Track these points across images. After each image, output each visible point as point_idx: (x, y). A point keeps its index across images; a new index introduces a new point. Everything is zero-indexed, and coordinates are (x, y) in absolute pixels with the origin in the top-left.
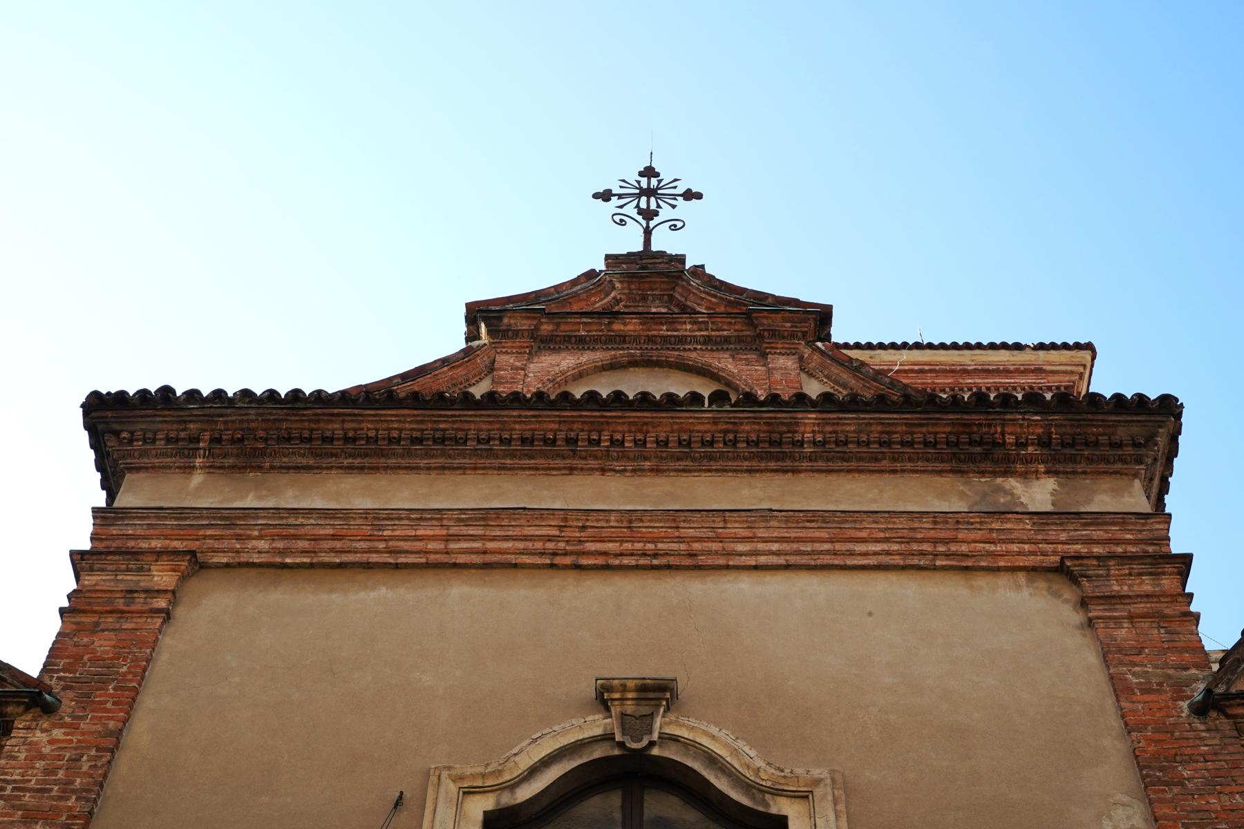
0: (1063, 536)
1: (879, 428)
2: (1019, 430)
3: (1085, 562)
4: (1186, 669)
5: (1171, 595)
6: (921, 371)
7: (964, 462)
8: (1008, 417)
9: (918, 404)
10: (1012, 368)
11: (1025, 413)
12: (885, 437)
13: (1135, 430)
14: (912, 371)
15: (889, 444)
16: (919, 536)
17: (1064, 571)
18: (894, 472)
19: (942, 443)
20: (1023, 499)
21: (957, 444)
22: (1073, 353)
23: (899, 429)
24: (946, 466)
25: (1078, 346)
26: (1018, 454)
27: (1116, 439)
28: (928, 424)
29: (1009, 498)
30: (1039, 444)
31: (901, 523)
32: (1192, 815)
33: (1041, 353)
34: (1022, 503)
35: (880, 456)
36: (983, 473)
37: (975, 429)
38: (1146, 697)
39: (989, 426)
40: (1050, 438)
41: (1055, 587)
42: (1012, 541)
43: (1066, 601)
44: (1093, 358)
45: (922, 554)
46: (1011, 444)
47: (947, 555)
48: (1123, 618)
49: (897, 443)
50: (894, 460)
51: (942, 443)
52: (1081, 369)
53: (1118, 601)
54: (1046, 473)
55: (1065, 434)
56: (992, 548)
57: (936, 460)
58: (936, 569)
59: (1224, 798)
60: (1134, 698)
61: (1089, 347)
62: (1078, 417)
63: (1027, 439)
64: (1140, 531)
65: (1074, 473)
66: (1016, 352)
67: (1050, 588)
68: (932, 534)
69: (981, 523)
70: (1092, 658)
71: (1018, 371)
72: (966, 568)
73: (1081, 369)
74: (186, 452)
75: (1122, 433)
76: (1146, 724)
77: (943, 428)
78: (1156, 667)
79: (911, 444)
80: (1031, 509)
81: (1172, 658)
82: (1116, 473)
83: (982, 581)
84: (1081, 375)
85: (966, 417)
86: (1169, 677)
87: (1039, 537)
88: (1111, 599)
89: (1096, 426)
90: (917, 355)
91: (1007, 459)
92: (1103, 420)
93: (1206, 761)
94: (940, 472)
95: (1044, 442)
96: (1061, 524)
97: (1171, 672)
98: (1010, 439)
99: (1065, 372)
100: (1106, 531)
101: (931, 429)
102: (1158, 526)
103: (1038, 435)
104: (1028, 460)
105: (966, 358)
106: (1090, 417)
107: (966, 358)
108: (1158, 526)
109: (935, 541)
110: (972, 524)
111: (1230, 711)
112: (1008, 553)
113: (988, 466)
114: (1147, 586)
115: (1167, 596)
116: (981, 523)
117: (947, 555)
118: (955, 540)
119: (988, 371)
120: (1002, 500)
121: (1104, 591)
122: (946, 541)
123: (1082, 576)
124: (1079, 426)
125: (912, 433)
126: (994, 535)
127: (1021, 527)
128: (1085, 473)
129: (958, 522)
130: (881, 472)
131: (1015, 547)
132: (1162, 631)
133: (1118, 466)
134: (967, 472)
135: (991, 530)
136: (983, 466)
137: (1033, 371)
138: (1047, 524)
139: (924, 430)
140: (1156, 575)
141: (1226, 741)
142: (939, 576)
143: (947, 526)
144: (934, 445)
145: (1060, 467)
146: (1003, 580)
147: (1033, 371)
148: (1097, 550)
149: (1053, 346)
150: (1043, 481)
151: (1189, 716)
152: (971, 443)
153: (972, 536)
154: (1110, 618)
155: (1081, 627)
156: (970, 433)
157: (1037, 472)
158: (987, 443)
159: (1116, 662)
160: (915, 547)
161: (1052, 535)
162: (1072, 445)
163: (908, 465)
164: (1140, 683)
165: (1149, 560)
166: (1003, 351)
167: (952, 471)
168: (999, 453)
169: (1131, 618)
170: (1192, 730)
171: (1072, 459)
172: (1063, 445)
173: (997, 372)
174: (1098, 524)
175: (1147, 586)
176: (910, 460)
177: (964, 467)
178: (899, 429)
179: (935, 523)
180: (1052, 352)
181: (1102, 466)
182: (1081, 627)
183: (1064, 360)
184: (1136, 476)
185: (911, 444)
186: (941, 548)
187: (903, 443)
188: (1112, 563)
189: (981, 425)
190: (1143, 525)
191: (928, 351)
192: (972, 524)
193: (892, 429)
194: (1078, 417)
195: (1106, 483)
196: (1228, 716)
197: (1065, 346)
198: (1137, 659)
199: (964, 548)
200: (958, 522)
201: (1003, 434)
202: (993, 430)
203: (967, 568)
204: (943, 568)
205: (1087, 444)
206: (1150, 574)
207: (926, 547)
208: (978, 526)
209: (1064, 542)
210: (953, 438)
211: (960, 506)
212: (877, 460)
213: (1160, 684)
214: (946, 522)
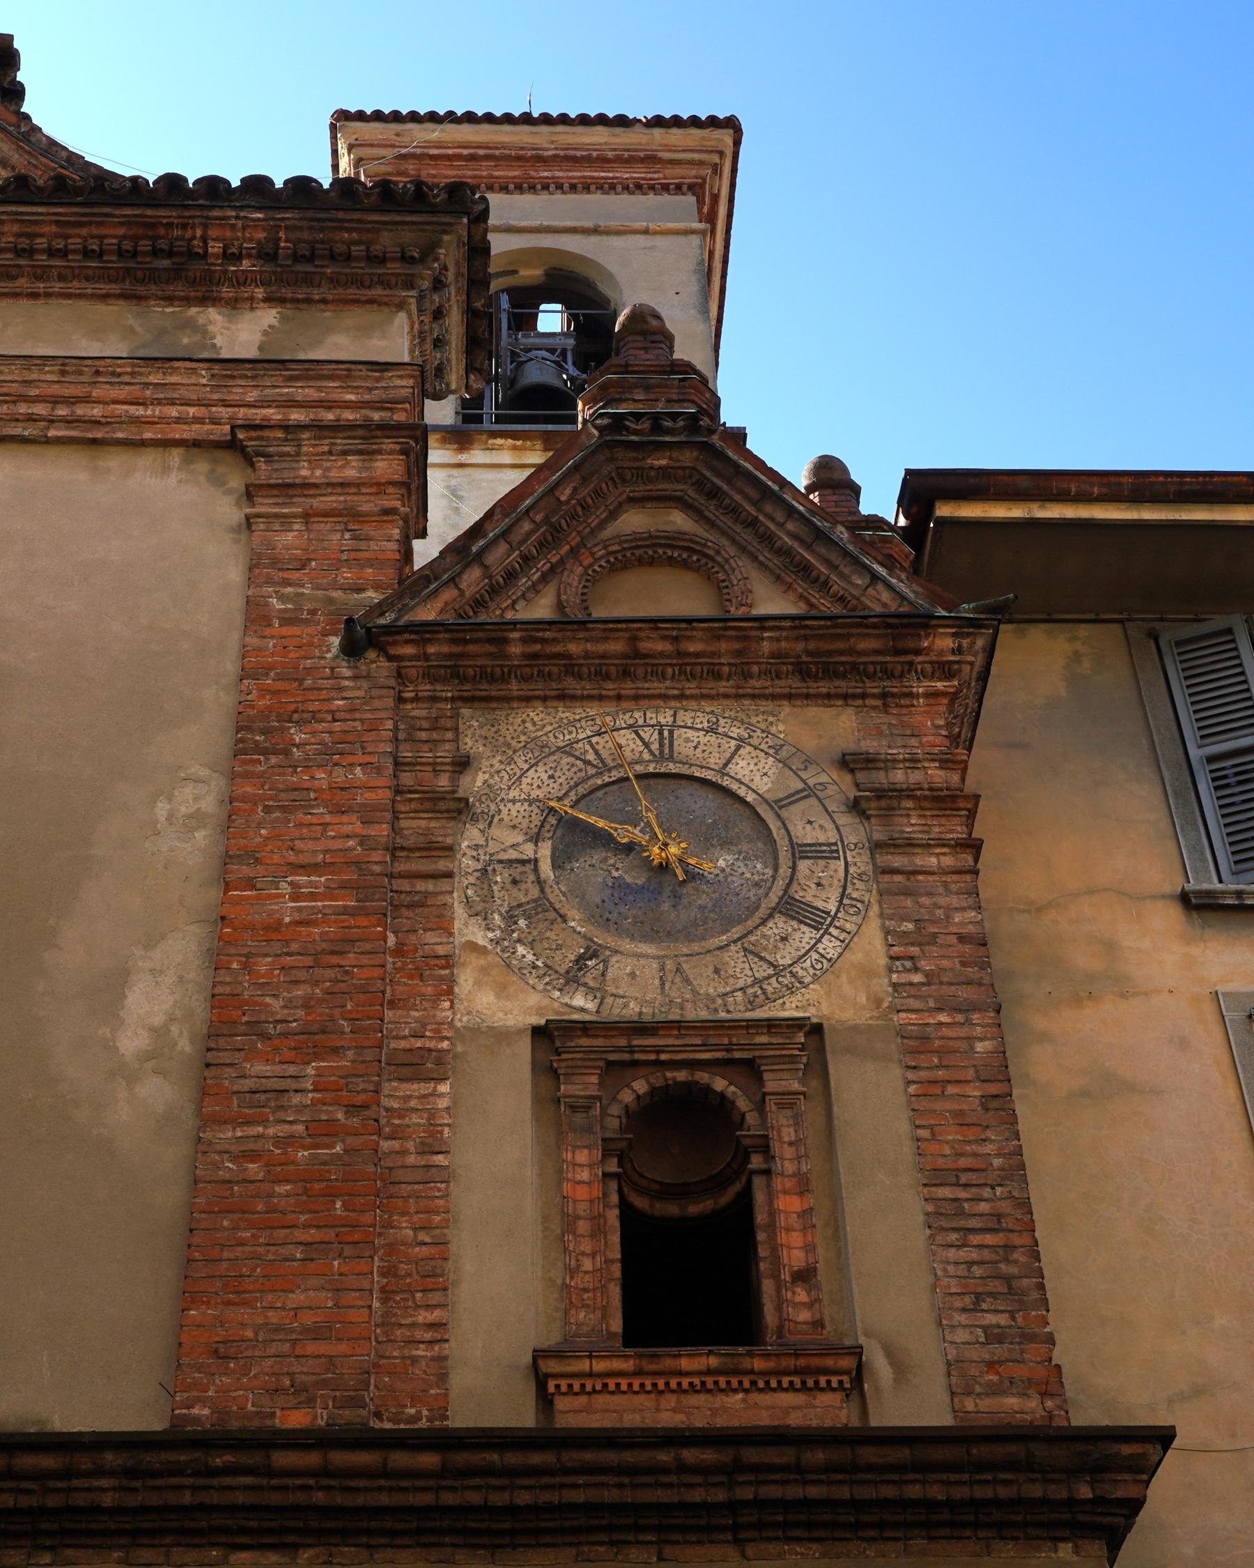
0: (252, 396)
1: (16, 228)
2: (228, 234)
3: (267, 433)
4: (360, 590)
5: (379, 484)
6: (472, 158)
7: (142, 281)
8: (216, 213)
9: (78, 191)
10: (610, 154)
11: (242, 208)
12: (24, 243)
13: (407, 236)
14: (459, 157)
15: (30, 252)
16: (34, 392)
17: (235, 446)
18: (34, 296)
19: (110, 252)
20: (218, 341)
21: (135, 254)
22: (705, 133)
23: (46, 229)
24: (115, 288)
25: (713, 122)
26: (226, 272)
27: (376, 249)
28: (90, 223)
29: (198, 337)
30: (259, 257)
31: (11, 372)
32: (283, 796)
33: (657, 132)
34: (214, 346)
35: (14, 272)
36: (170, 300)
37: (162, 231)
38: (287, 630)
39: (184, 226)
40: (277, 247)
41: (221, 469)
42: (172, 402)
43: (229, 492)
44: (737, 143)
45: (31, 419)
46: (216, 256)
47: (68, 422)
48: (295, 516)
49: (42, 251)
50: (39, 278)
51: (110, 252)
52: (716, 159)
53: (298, 491)
54: (265, 300)
55: (300, 241)
56: (140, 411)
57: (100, 279)
58: (48, 441)
59: (339, 771)
60: (267, 631)
61: (732, 124)
62: (323, 215)
63: (241, 248)
64: (370, 389)
65: (308, 301)
66: (618, 130)
67: (212, 471)
68: (55, 389)
69: (132, 374)
70: (235, 574)
71: (619, 160)
72: (93, 441)
73: (716, 159)
74: (139, 273)
75: (386, 241)
76: (271, 667)
77: (113, 229)
78: (317, 587)
79: (64, 253)
80: (225, 354)
81: (347, 575)
82: (371, 301)
83: (114, 461)
84: (716, 169)
85: (149, 212)
86: (331, 601)
87: (216, 396)
88: (287, 489)
89: (350, 230)
90: (466, 133)
91: (209, 279)
92: (360, 221)
93: (335, 720)
94: (105, 297)
95: (267, 254)
96: (254, 377)
97: (336, 594)
98: (215, 248)
99: (691, 163)
100: (319, 389)
101: (95, 231)
102: (399, 382)
103: (259, 242)
104: (242, 280)
105: (541, 138)
106: (341, 215)
107: (541, 138)
108: (399, 382)
109: (55, 401)
110: (119, 375)
111: (392, 651)
112: (162, 420)
113: (179, 289)
114: (352, 470)
115: (371, 486)
116: (132, 374)
117: (68, 422)
118: (86, 400)
119: (575, 159)
120: (185, 341)
121: (288, 477)
122: (71, 401)
123: (258, 454)
124: (321, 230)
125: (66, 237)
126: (148, 393)
127: (193, 381)
128: (324, 301)
129: (97, 373)
130: (15, 295)
131: (173, 412)
132: (347, 536)
133: (377, 292)
134: (146, 298)
135: (147, 384)
136: (170, 289)
137: (642, 160)
138: (233, 377)
139: (84, 231)
140: (368, 454)
141: (375, 692)
142: (51, 452)
143: (82, 379)
144: (100, 255)
145: (287, 292)
146: (148, 458)
147: (642, 160)
148: (297, 416)
149: (676, 121)
150: (259, 313)
151: (337, 657)
152: (156, 252)
153: (115, 393)
154: (277, 516)
155: (237, 530)
156: (155, 238)
157: (252, 299)
158: (180, 254)
159: (262, 579)
160: (23, 409)
161: (236, 394)
162: (310, 259)
163: (57, 286)
164: (285, 611)
165: (360, 432)
166: (600, 128)
167: (124, 296)
168: (197, 268)
169: (307, 516)
170: (333, 676)
171: (308, 280)
172: (296, 258)
173: (587, 161)
174: (309, 378)
175: (352, 470)
176: (61, 278)
177: (141, 290)
178: (46, 229)
179: (63, 373)
180: (674, 130)
181: (352, 292)
182: (237, 530)
183: (691, 143)
184: (401, 306)
185: (64, 253)
186: (62, 411)
187: (51, 253)
188: (306, 435)
189: (170, 225)
190: (378, 380)
191: (486, 127)
192: (119, 375)
193: (36, 229)
194: (323, 215)
195: (355, 316)
196: (390, 658)
197: (694, 121)
198: (294, 575)
199: (96, 412)
200: (97, 373)
201: (204, 239)
202: (189, 234)
203: (94, 442)
204: (59, 441)
205: (333, 257)
206: (360, 452)
207: (40, 409)
208: (127, 379)
209: (253, 402)
210: (127, 245)
211: (118, 348)
212: (12, 278)
213: (313, 612)
214: (80, 373)
